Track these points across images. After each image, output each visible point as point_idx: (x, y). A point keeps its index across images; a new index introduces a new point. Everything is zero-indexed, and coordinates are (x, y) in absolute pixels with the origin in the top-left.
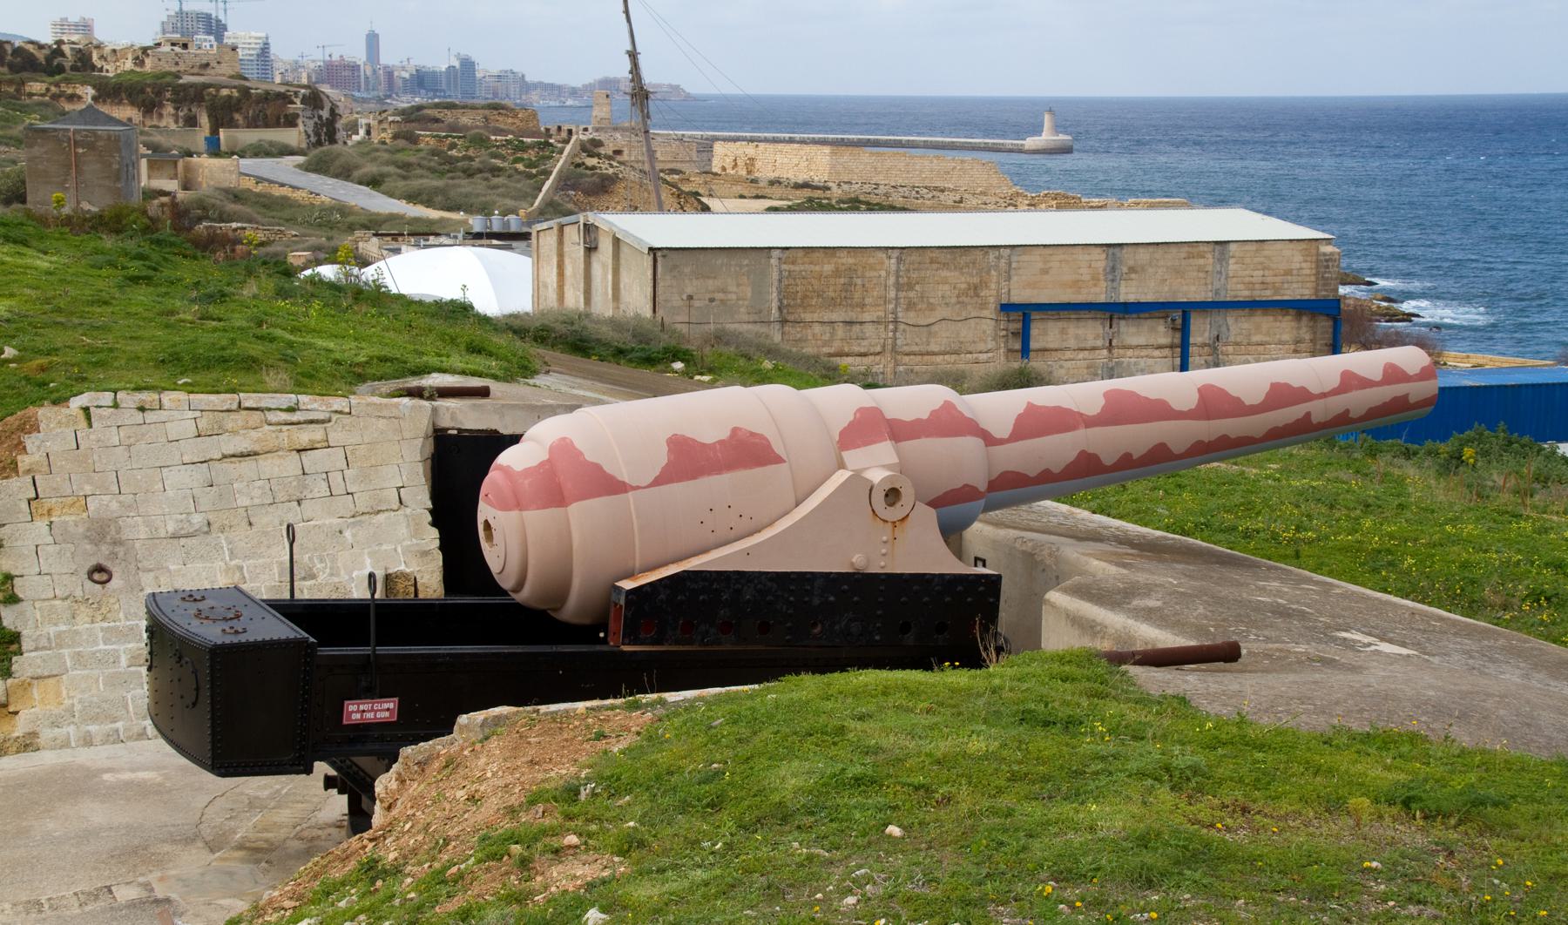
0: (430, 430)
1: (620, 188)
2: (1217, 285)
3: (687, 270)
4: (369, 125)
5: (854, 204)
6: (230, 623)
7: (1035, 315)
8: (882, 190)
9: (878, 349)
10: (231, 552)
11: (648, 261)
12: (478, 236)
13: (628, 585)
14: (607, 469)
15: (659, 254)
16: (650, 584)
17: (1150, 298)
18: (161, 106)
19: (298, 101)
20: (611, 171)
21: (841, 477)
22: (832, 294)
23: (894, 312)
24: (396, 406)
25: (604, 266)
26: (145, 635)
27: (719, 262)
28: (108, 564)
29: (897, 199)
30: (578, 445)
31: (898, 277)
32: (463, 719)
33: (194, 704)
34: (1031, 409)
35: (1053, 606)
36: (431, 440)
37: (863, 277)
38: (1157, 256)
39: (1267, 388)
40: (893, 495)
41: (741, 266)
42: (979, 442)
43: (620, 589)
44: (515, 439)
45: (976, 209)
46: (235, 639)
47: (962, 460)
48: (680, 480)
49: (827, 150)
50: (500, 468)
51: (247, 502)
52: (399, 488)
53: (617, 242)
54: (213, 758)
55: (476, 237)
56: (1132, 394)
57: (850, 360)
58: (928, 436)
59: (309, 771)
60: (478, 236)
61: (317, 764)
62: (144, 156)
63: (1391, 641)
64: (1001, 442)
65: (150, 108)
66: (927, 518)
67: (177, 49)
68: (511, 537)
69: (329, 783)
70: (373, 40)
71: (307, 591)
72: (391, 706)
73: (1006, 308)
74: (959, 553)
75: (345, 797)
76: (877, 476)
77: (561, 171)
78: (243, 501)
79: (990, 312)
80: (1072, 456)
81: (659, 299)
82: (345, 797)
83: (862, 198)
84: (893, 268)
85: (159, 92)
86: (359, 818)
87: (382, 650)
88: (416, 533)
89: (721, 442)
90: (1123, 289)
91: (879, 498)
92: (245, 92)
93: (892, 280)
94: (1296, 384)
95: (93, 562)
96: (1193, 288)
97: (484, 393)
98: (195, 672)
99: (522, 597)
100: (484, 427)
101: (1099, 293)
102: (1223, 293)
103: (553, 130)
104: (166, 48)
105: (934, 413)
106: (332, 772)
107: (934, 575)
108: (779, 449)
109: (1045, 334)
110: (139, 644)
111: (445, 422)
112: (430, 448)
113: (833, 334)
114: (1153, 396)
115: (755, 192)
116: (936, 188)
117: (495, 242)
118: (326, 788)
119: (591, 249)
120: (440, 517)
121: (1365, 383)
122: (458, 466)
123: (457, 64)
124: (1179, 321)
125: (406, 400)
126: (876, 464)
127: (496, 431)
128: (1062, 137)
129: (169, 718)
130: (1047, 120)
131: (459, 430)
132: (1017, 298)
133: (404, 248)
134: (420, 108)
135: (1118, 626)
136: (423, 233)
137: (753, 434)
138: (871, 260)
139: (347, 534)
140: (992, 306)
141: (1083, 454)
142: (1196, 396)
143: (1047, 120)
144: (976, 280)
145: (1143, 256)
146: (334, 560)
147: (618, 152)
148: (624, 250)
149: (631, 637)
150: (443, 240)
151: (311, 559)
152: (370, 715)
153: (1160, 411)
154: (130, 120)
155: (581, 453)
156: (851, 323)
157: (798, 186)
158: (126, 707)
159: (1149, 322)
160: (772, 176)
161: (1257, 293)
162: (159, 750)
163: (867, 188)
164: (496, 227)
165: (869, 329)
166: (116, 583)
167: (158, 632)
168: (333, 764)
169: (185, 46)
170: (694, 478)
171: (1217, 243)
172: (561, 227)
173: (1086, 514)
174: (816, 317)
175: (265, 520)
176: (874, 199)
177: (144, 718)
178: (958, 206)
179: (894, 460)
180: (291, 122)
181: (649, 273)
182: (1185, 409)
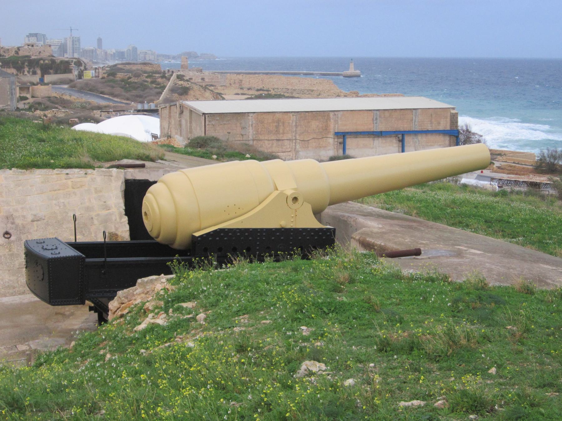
0: (124, 181)
1: (191, 92)
4: (26, 99)
5: (269, 96)
6: (54, 251)
8: (290, 91)
11: (203, 117)
15: (207, 116)
18: (24, 68)
19: (73, 64)
20: (188, 86)
25: (186, 121)
26: (24, 256)
28: (11, 231)
32: (139, 281)
33: (43, 279)
36: (124, 184)
40: (295, 199)
44: (155, 182)
46: (56, 256)
54: (50, 298)
55: (139, 111)
59: (83, 303)
61: (87, 302)
62: (17, 86)
63: (475, 249)
65: (20, 69)
67: (30, 47)
69: (91, 309)
70: (100, 41)
71: (81, 239)
73: (337, 134)
74: (320, 221)
75: (97, 314)
79: (331, 135)
82: (97, 314)
85: (23, 63)
86: (102, 319)
87: (108, 259)
88: (121, 218)
92: (53, 61)
93: (294, 124)
95: (4, 231)
97: (143, 166)
98: (42, 268)
99: (159, 240)
100: (143, 178)
103: (166, 72)
104: (26, 47)
106: (93, 305)
110: (22, 259)
111: (129, 177)
112: (123, 188)
113: (272, 144)
117: (145, 113)
119: (182, 112)
120: (128, 212)
122: (135, 193)
123: (131, 49)
130: (352, 66)
134: (116, 65)
136: (120, 111)
143: (352, 66)
147: (191, 79)
148: (194, 115)
154: (13, 73)
157: (258, 90)
160: (248, 86)
162: (31, 298)
163: (284, 90)
164: (146, 107)
165: (286, 143)
166: (12, 238)
167: (31, 257)
168: (93, 302)
169: (33, 46)
174: (266, 138)
176: (286, 95)
177: (24, 287)
180: (70, 71)
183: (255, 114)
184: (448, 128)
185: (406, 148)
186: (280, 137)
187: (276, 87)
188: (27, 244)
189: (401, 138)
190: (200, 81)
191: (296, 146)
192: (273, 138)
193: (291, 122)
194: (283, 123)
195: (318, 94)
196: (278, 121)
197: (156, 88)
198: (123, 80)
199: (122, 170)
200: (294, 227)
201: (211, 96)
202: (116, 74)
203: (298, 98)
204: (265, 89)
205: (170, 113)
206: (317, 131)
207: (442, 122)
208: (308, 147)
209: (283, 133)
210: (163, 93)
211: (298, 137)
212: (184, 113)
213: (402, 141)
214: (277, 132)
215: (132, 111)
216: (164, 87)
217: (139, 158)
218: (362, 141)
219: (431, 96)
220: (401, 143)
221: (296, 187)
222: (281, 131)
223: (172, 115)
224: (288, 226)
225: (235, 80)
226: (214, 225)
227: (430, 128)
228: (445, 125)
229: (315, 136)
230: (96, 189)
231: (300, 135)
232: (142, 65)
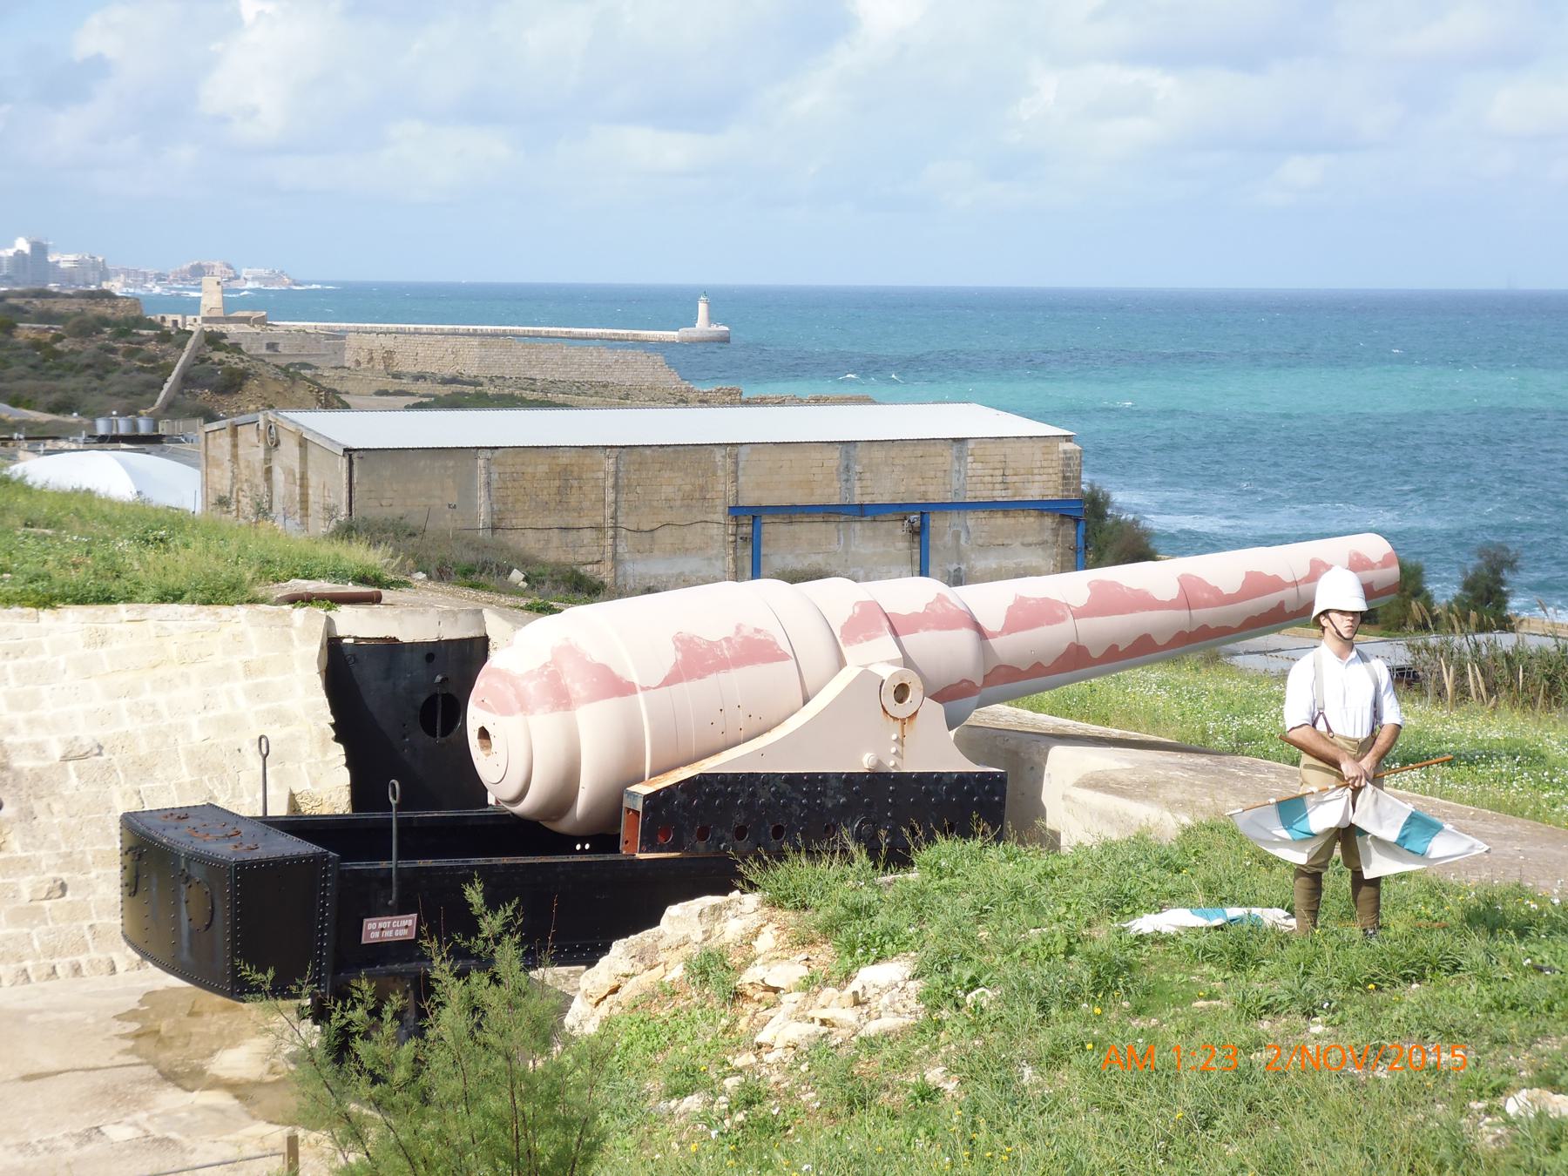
1: (252, 384)
2: (956, 485)
5: (482, 401)
11: (345, 461)
12: (103, 439)
13: (643, 789)
14: (618, 672)
15: (355, 455)
22: (546, 498)
27: (422, 463)
34: (1020, 602)
37: (580, 478)
38: (893, 454)
39: (1243, 578)
40: (901, 692)
47: (951, 651)
49: (475, 342)
50: (498, 672)
53: (303, 443)
56: (1115, 584)
57: (589, 568)
58: (927, 629)
60: (103, 439)
64: (994, 635)
66: (935, 712)
72: (410, 922)
73: (736, 511)
76: (888, 672)
77: (183, 366)
84: (612, 468)
91: (889, 700)
93: (610, 482)
94: (1269, 572)
97: (375, 600)
101: (832, 494)
113: (548, 541)
126: (878, 658)
128: (714, 327)
129: (150, 941)
130: (702, 308)
132: (748, 500)
133: (21, 454)
138: (588, 461)
140: (720, 509)
143: (702, 308)
144: (701, 481)
145: (878, 454)
148: (313, 453)
149: (649, 845)
150: (62, 444)
152: (388, 934)
153: (1145, 602)
157: (445, 382)
158: (30, 943)
161: (996, 493)
172: (235, 428)
173: (1029, 714)
174: (528, 522)
176: (529, 395)
182: (1168, 599)
186: (570, 519)
187: (498, 373)
188: (130, 822)
189: (917, 524)
190: (264, 351)
191: (615, 546)
192: (549, 522)
195: (622, 394)
197: (141, 369)
198: (36, 345)
199: (321, 611)
201: (311, 398)
202: (15, 327)
203: (564, 406)
204: (465, 378)
205: (235, 446)
210: (166, 386)
213: (919, 533)
215: (81, 439)
216: (169, 368)
217: (363, 580)
223: (241, 451)
225: (371, 352)
226: (685, 764)
230: (246, 664)
232: (83, 301)
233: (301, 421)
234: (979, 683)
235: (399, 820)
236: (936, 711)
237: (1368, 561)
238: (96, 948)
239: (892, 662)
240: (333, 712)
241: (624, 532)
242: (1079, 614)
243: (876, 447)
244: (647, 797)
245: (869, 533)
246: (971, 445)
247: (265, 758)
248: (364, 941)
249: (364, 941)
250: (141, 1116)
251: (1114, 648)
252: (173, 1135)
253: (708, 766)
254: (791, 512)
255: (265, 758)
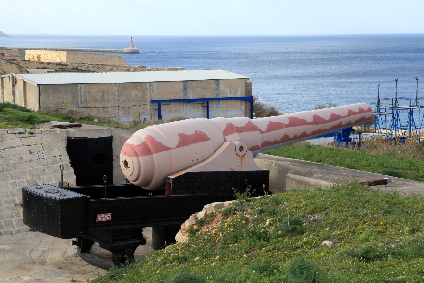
3: (50, 92)
5: (76, 70)
7: (162, 104)
9: (114, 115)
10: (11, 177)
13: (172, 177)
14: (164, 143)
15: (41, 86)
16: (179, 176)
17: (197, 97)
21: (227, 144)
23: (118, 104)
24: (56, 131)
29: (91, 68)
30: (154, 137)
31: (119, 92)
35: (290, 178)
39: (330, 115)
40: (241, 148)
41: (68, 90)
42: (259, 132)
43: (170, 178)
45: (117, 71)
48: (183, 146)
51: (14, 162)
52: (60, 156)
53: (25, 83)
58: (246, 131)
68: (129, 165)
72: (109, 215)
73: (153, 101)
76: (237, 143)
78: (13, 162)
79: (148, 103)
80: (282, 136)
81: (41, 101)
83: (79, 68)
87: (108, 199)
89: (193, 135)
90: (188, 95)
94: (337, 114)
96: (209, 94)
97: (80, 126)
102: (218, 95)
105: (246, 125)
107: (252, 171)
108: (208, 136)
109: (164, 108)
113: (99, 111)
114: (301, 118)
115: (43, 67)
116: (103, 65)
118: (73, 245)
121: (355, 113)
124: (206, 104)
125: (58, 129)
126: (235, 139)
127: (86, 138)
131: (75, 138)
132: (156, 99)
135: (314, 182)
137: (201, 132)
139: (46, 170)
141: (285, 135)
142: (312, 118)
146: (43, 179)
148: (28, 86)
151: (36, 179)
152: (104, 219)
155: (155, 139)
156: (103, 107)
159: (197, 105)
163: (80, 65)
165: (110, 109)
170: (187, 145)
171: (216, 80)
175: (20, 167)
176: (84, 69)
178: (111, 70)
179: (239, 138)
181: (38, 93)
183: (83, 85)
184: (244, 95)
185: (211, 113)
186: (106, 105)
187: (72, 62)
188: (23, 189)
192: (99, 105)
193: (114, 91)
194: (108, 92)
196: (103, 91)
200: (240, 170)
206: (137, 99)
207: (239, 91)
208: (129, 113)
209: (108, 102)
211: (120, 105)
212: (18, 84)
214: (103, 101)
218: (174, 107)
219: (231, 70)
220: (206, 109)
221: (239, 138)
222: (106, 100)
224: (237, 170)
226: (183, 170)
227: (229, 96)
228: (241, 93)
229: (134, 103)
231: (122, 103)
233: (23, 76)
234: (260, 146)
235: (104, 187)
236: (250, 153)
237: (364, 110)
238: (6, 227)
239: (238, 140)
240: (70, 159)
241: (121, 108)
242: (287, 126)
243: (193, 82)
244: (173, 179)
245: (192, 107)
246: (220, 81)
247: (62, 171)
248: (97, 221)
249: (97, 221)
250: (31, 273)
251: (296, 136)
252: (42, 278)
253: (190, 170)
254: (164, 101)
255: (62, 171)
